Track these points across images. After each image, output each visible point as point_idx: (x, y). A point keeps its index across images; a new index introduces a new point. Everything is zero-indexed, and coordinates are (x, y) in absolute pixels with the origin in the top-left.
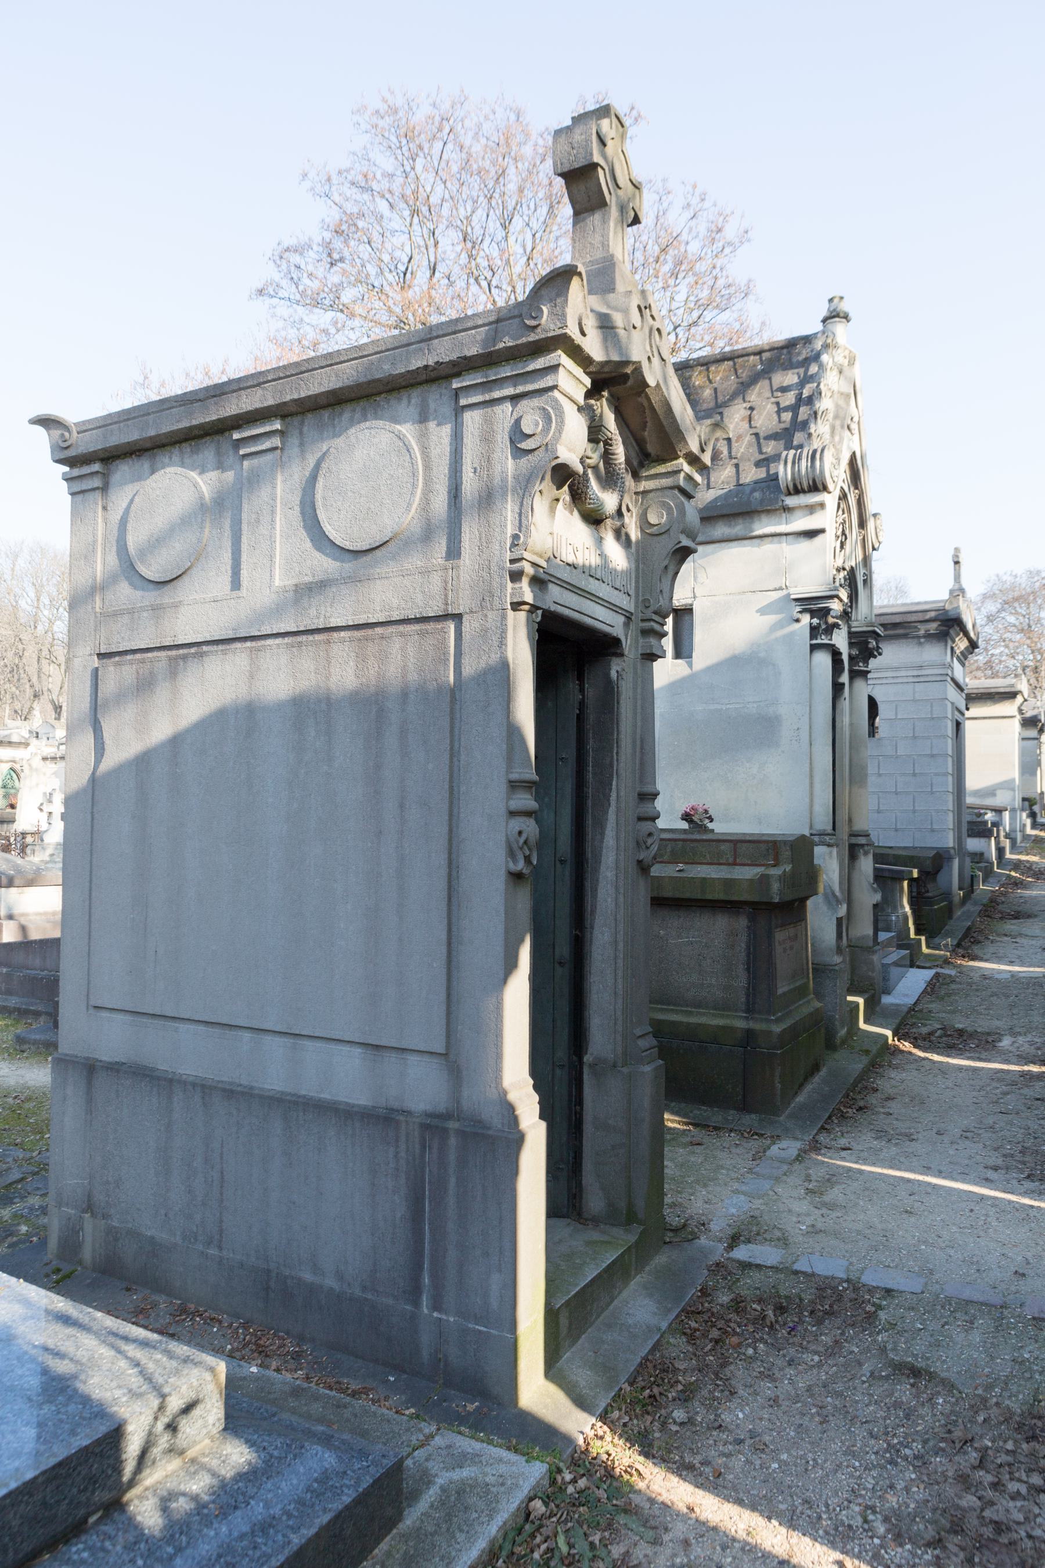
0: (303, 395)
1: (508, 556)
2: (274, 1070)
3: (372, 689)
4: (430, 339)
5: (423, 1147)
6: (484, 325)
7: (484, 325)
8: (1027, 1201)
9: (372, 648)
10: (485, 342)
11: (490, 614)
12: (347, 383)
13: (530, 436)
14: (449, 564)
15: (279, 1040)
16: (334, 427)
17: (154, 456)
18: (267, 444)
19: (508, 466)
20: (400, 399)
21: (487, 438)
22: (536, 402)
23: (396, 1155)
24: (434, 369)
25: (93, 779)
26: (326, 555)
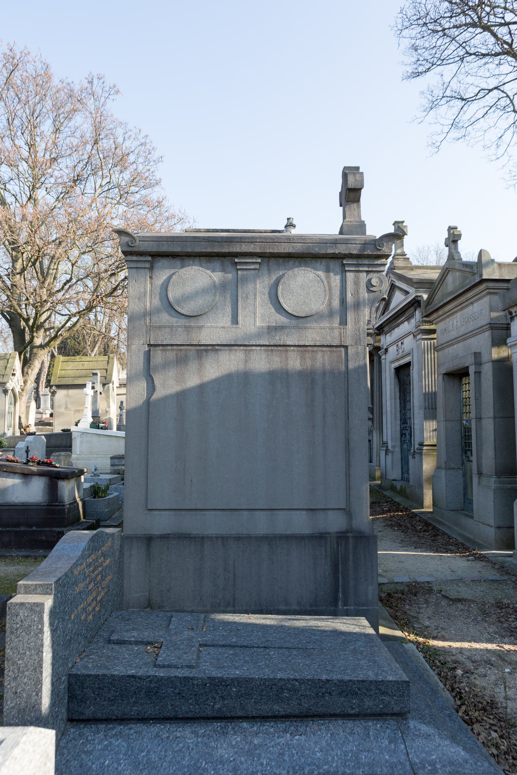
0: (275, 251)
1: (366, 327)
2: (261, 525)
3: (309, 371)
4: (336, 244)
5: (338, 545)
6: (359, 244)
7: (359, 244)
8: (421, 553)
9: (308, 355)
10: (360, 250)
11: (359, 347)
12: (298, 251)
13: (375, 286)
14: (342, 327)
15: (264, 513)
16: (285, 266)
17: (184, 260)
18: (252, 267)
19: (364, 294)
20: (317, 262)
21: (356, 283)
22: (376, 275)
23: (326, 551)
24: (337, 254)
25: (148, 403)
26: (283, 316)
